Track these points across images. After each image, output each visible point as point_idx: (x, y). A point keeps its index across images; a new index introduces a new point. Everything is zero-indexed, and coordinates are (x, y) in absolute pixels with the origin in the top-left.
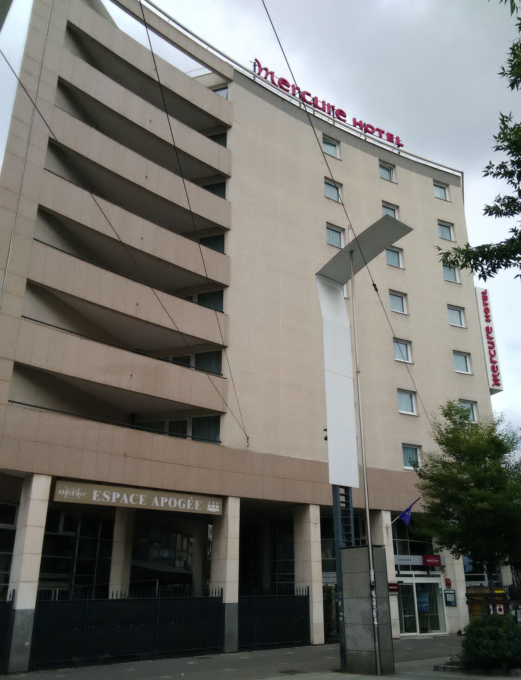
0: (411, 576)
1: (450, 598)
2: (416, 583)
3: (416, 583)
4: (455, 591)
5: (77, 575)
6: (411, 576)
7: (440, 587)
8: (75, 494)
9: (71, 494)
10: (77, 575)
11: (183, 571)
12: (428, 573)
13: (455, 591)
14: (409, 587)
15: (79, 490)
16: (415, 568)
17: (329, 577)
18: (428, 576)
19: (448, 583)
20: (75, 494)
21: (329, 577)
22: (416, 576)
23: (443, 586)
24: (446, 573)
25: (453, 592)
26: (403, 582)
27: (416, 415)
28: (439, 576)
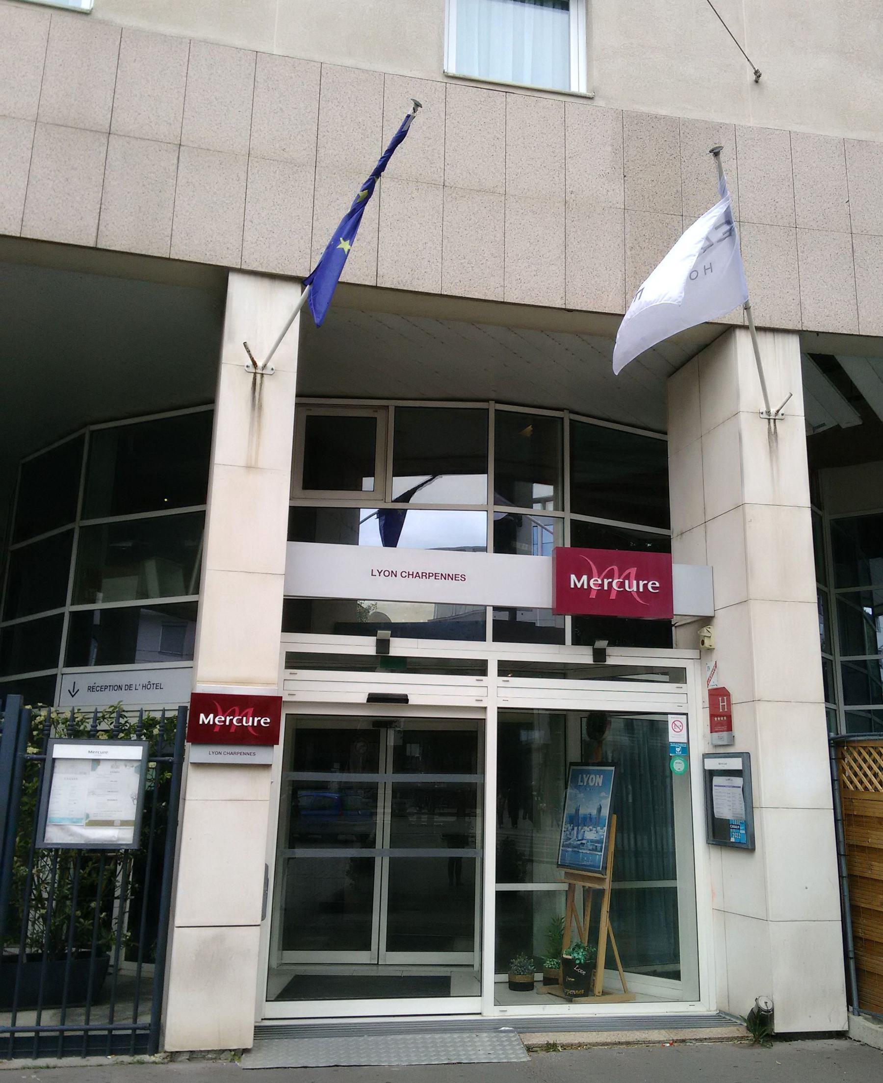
0: (478, 668)
1: (728, 807)
2: (503, 713)
3: (503, 713)
4: (746, 757)
5: (400, 853)
6: (478, 668)
7: (674, 736)
8: (622, 585)
9: (610, 584)
10: (400, 853)
11: (569, 810)
12: (600, 655)
13: (746, 757)
14: (453, 741)
15: (633, 571)
16: (513, 626)
17: (129, 687)
18: (600, 671)
19: (721, 716)
20: (622, 585)
21: (129, 687)
22: (507, 669)
23: (691, 733)
24: (716, 656)
25: (736, 764)
26: (402, 699)
27: (583, 90)
28: (677, 675)
